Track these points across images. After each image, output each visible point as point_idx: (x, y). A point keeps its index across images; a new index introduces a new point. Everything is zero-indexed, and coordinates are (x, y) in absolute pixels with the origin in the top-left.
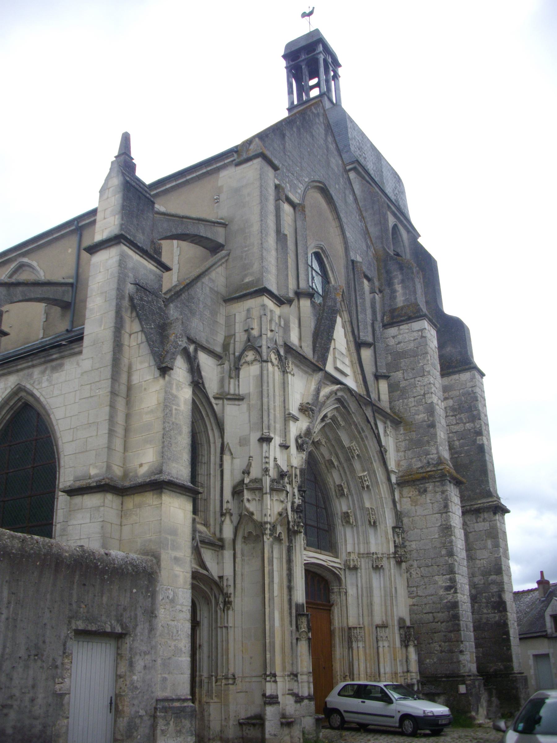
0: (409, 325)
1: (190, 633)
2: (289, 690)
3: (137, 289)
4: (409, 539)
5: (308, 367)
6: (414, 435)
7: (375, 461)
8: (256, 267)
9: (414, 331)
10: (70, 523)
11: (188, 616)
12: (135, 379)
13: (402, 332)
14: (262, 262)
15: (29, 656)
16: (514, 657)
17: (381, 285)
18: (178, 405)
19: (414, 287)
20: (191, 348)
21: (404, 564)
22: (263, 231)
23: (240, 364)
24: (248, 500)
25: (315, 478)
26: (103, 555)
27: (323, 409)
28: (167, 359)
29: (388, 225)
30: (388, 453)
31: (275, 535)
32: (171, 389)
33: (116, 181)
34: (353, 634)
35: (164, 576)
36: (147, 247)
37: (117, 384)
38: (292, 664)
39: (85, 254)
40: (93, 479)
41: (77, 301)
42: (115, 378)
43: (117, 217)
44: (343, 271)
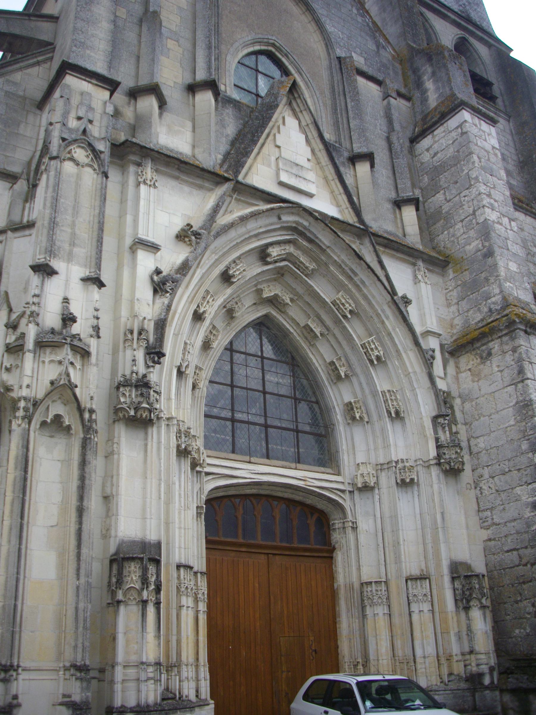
0: (445, 125)
2: (64, 696)
4: (474, 435)
6: (467, 276)
7: (388, 318)
9: (451, 132)
13: (437, 139)
25: (293, 358)
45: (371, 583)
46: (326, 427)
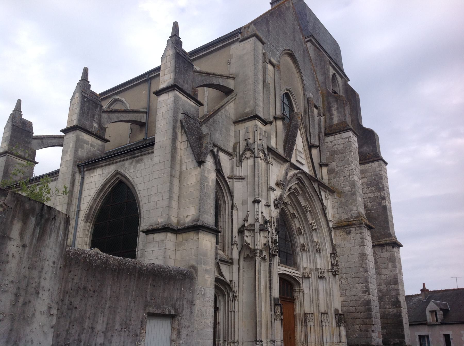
0: (341, 134)
1: (213, 315)
3: (185, 116)
4: (340, 261)
5: (281, 160)
6: (343, 199)
7: (320, 215)
8: (252, 103)
9: (343, 138)
10: (146, 250)
11: (212, 304)
12: (184, 168)
13: (336, 139)
14: (255, 100)
15: (121, 329)
16: (406, 335)
17: (324, 111)
18: (208, 182)
19: (344, 112)
20: (215, 150)
21: (337, 276)
22: (255, 83)
23: (243, 159)
24: (247, 236)
25: (285, 224)
26: (165, 269)
27: (289, 184)
28: (202, 157)
29: (330, 75)
30: (327, 210)
31: (262, 256)
32: (205, 173)
33: (171, 52)
34: (307, 317)
35: (199, 280)
36: (190, 92)
37: (174, 170)
38: (272, 334)
39: (153, 96)
40: (160, 225)
41: (149, 122)
42: (172, 167)
43: (172, 74)
44: (302, 103)
45: (309, 313)
46: (293, 251)
